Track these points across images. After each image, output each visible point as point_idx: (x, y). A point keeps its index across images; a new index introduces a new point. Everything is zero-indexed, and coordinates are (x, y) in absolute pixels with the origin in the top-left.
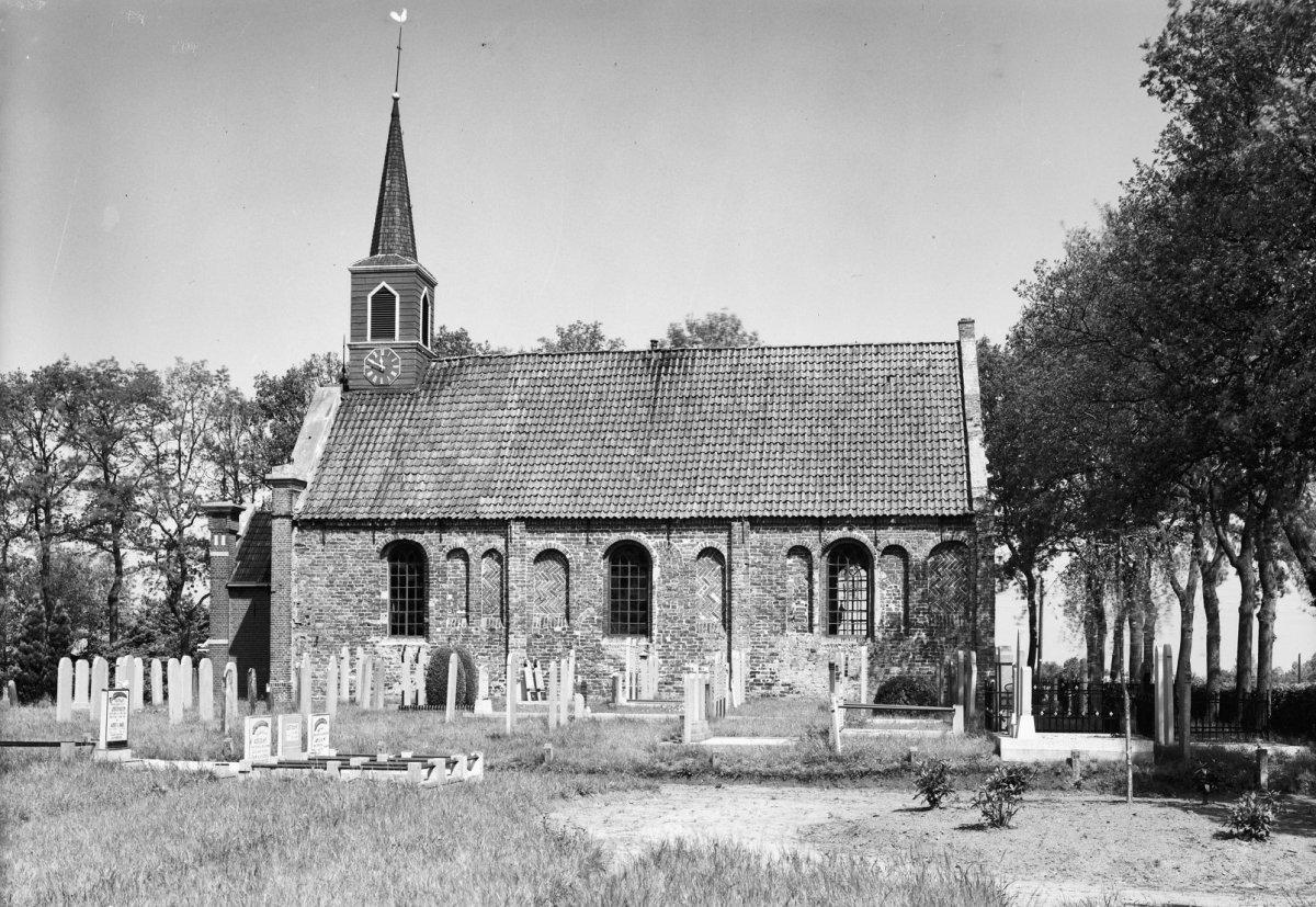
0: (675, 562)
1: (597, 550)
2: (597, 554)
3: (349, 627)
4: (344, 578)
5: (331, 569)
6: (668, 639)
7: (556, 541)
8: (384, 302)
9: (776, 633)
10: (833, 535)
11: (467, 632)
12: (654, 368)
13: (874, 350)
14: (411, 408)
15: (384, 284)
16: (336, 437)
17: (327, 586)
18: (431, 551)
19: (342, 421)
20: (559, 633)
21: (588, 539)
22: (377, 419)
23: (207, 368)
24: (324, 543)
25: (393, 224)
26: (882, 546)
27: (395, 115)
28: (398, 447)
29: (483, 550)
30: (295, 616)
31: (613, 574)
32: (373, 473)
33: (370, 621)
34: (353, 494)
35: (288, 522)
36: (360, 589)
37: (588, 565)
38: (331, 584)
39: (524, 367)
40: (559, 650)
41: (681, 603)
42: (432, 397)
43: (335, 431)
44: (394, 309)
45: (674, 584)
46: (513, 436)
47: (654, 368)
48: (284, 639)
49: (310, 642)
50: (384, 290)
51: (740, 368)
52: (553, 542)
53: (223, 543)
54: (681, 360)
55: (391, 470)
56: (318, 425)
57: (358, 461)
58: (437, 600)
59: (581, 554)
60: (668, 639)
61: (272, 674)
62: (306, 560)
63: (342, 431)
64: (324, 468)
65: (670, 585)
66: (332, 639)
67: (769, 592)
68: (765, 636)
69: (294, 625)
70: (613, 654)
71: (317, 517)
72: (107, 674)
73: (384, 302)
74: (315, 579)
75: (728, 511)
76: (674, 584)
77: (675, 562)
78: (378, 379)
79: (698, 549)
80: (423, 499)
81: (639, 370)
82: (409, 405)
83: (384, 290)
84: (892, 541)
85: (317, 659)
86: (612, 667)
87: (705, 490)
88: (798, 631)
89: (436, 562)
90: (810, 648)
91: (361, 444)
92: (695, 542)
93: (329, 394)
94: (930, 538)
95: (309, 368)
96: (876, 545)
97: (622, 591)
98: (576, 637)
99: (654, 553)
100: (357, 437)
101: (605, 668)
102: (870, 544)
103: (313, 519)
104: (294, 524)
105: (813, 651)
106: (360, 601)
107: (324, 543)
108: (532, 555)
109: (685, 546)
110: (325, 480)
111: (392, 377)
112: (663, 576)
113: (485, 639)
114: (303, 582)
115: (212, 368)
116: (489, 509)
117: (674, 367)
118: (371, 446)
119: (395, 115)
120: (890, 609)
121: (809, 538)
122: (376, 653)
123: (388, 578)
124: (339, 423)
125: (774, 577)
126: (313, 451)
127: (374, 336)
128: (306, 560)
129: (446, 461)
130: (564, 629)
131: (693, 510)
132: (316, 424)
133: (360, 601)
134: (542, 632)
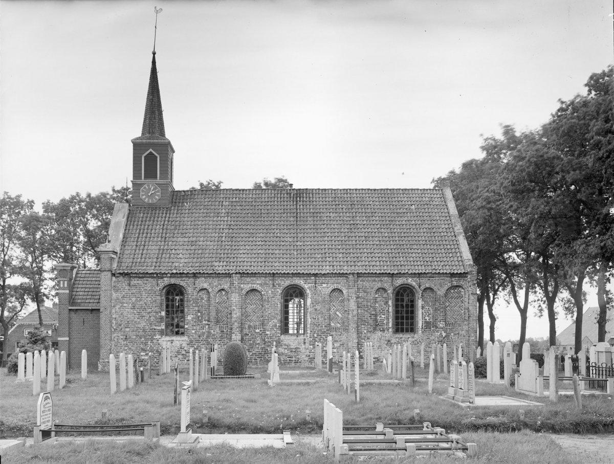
0: (319, 295)
1: (278, 290)
2: (278, 292)
3: (144, 331)
4: (141, 305)
5: (134, 299)
6: (315, 335)
7: (257, 284)
8: (151, 159)
9: (370, 332)
10: (399, 281)
11: (209, 332)
12: (293, 198)
13: (401, 192)
14: (168, 215)
15: (151, 150)
16: (129, 230)
17: (131, 309)
18: (190, 290)
19: (131, 222)
20: (258, 333)
21: (273, 284)
22: (149, 221)
23: (22, 199)
24: (130, 286)
25: (155, 119)
26: (422, 288)
27: (154, 62)
28: (164, 235)
29: (217, 289)
30: (113, 325)
31: (396, 314)
32: (153, 249)
33: (156, 327)
34: (143, 259)
35: (109, 274)
36: (149, 310)
37: (273, 297)
38: (134, 308)
39: (225, 196)
40: (258, 342)
41: (322, 317)
42: (178, 210)
43: (128, 226)
44: (141, 170)
45: (318, 307)
46: (226, 231)
47: (293, 198)
48: (108, 337)
49: (122, 339)
50: (151, 152)
51: (337, 199)
52: (255, 285)
53: (66, 286)
54: (306, 194)
55: (162, 247)
56: (117, 224)
57: (143, 243)
58: (192, 316)
59: (270, 292)
60: (315, 335)
61: (101, 356)
62: (120, 295)
63: (131, 227)
64: (125, 246)
65: (316, 307)
66: (134, 337)
67: (367, 311)
68: (365, 333)
69: (113, 330)
70: (287, 343)
71: (126, 272)
72: (27, 365)
73: (151, 159)
74: (125, 305)
75: (345, 270)
76: (318, 307)
77: (319, 295)
78: (149, 200)
79: (330, 289)
80: (182, 261)
81: (286, 199)
82: (166, 214)
83: (151, 152)
84: (427, 286)
85: (126, 348)
86: (286, 350)
87: (331, 259)
88: (381, 331)
89: (192, 296)
90: (387, 339)
91: (143, 233)
92: (329, 286)
93: (123, 207)
94: (445, 284)
95: (73, 198)
96: (420, 287)
97: (411, 328)
98: (267, 335)
99: (308, 291)
100: (140, 230)
101: (283, 350)
102: (417, 287)
103: (124, 272)
104: (113, 275)
105: (389, 341)
106: (150, 317)
107: (130, 286)
108: (244, 292)
109: (324, 288)
110: (126, 252)
111: (156, 199)
112: (313, 303)
113: (218, 336)
114: (118, 307)
115: (24, 199)
116: (220, 268)
117: (303, 198)
118: (149, 235)
119: (154, 62)
120: (426, 319)
121: (387, 283)
122: (159, 344)
123: (165, 304)
124: (129, 222)
125: (369, 304)
126: (118, 236)
127: (146, 177)
128: (120, 295)
129: (193, 243)
130: (261, 331)
131: (327, 269)
132: (118, 222)
133: (150, 317)
134: (249, 332)
